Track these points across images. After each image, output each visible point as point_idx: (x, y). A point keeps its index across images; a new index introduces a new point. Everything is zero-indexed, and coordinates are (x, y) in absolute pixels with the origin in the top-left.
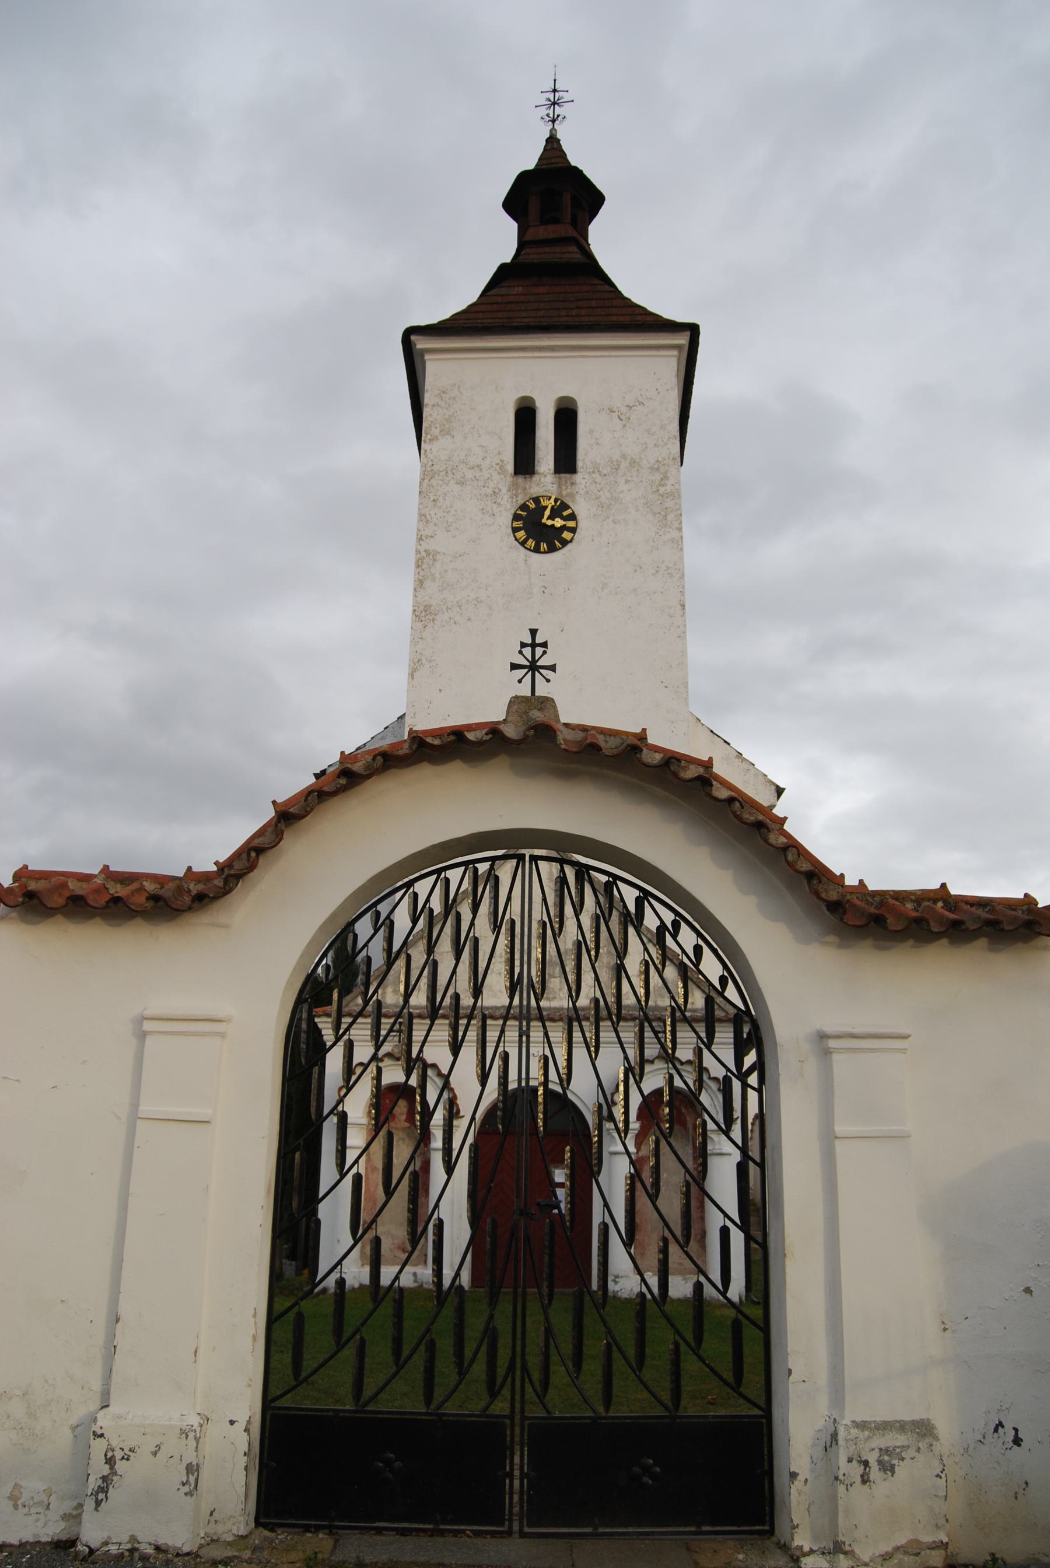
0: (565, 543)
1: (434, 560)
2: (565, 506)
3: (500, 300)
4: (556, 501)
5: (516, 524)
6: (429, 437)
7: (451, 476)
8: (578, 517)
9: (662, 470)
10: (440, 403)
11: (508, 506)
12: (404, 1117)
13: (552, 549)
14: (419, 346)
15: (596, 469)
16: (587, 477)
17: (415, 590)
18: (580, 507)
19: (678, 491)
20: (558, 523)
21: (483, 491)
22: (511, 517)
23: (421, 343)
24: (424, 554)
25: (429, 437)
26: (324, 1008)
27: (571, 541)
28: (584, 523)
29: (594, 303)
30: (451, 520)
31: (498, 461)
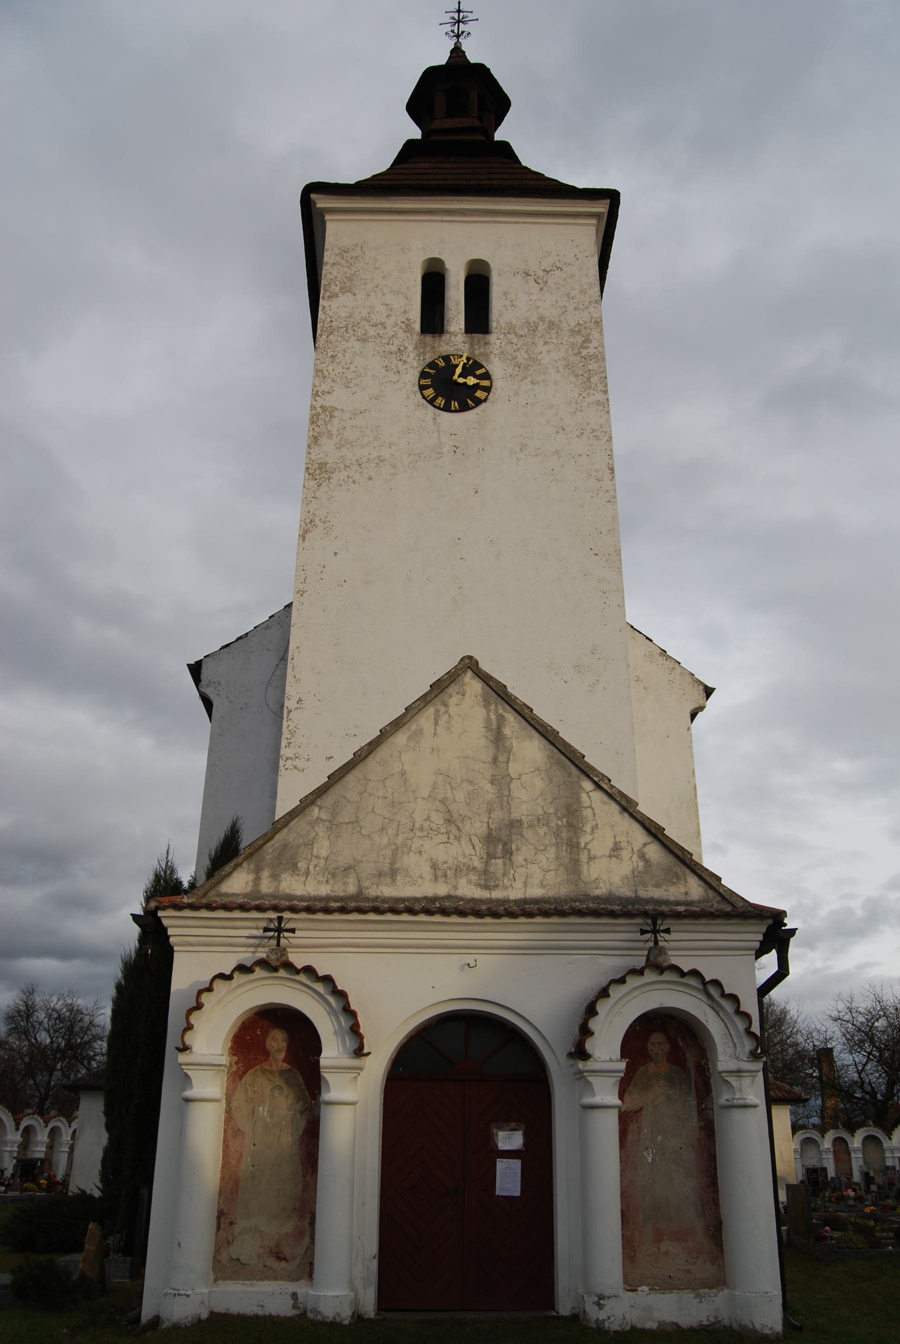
0: (478, 402)
1: (331, 417)
2: (478, 365)
3: (406, 171)
4: (468, 359)
5: (423, 382)
6: (328, 294)
7: (351, 332)
8: (493, 377)
9: (584, 332)
10: (341, 261)
11: (415, 364)
12: (282, 1056)
13: (464, 408)
14: (318, 206)
15: (512, 329)
16: (501, 337)
17: (309, 446)
18: (496, 367)
19: (602, 354)
20: (471, 381)
21: (387, 348)
22: (417, 375)
23: (321, 202)
24: (320, 410)
25: (328, 294)
26: (173, 898)
27: (485, 400)
28: (499, 383)
29: (506, 176)
30: (350, 375)
31: (404, 319)
